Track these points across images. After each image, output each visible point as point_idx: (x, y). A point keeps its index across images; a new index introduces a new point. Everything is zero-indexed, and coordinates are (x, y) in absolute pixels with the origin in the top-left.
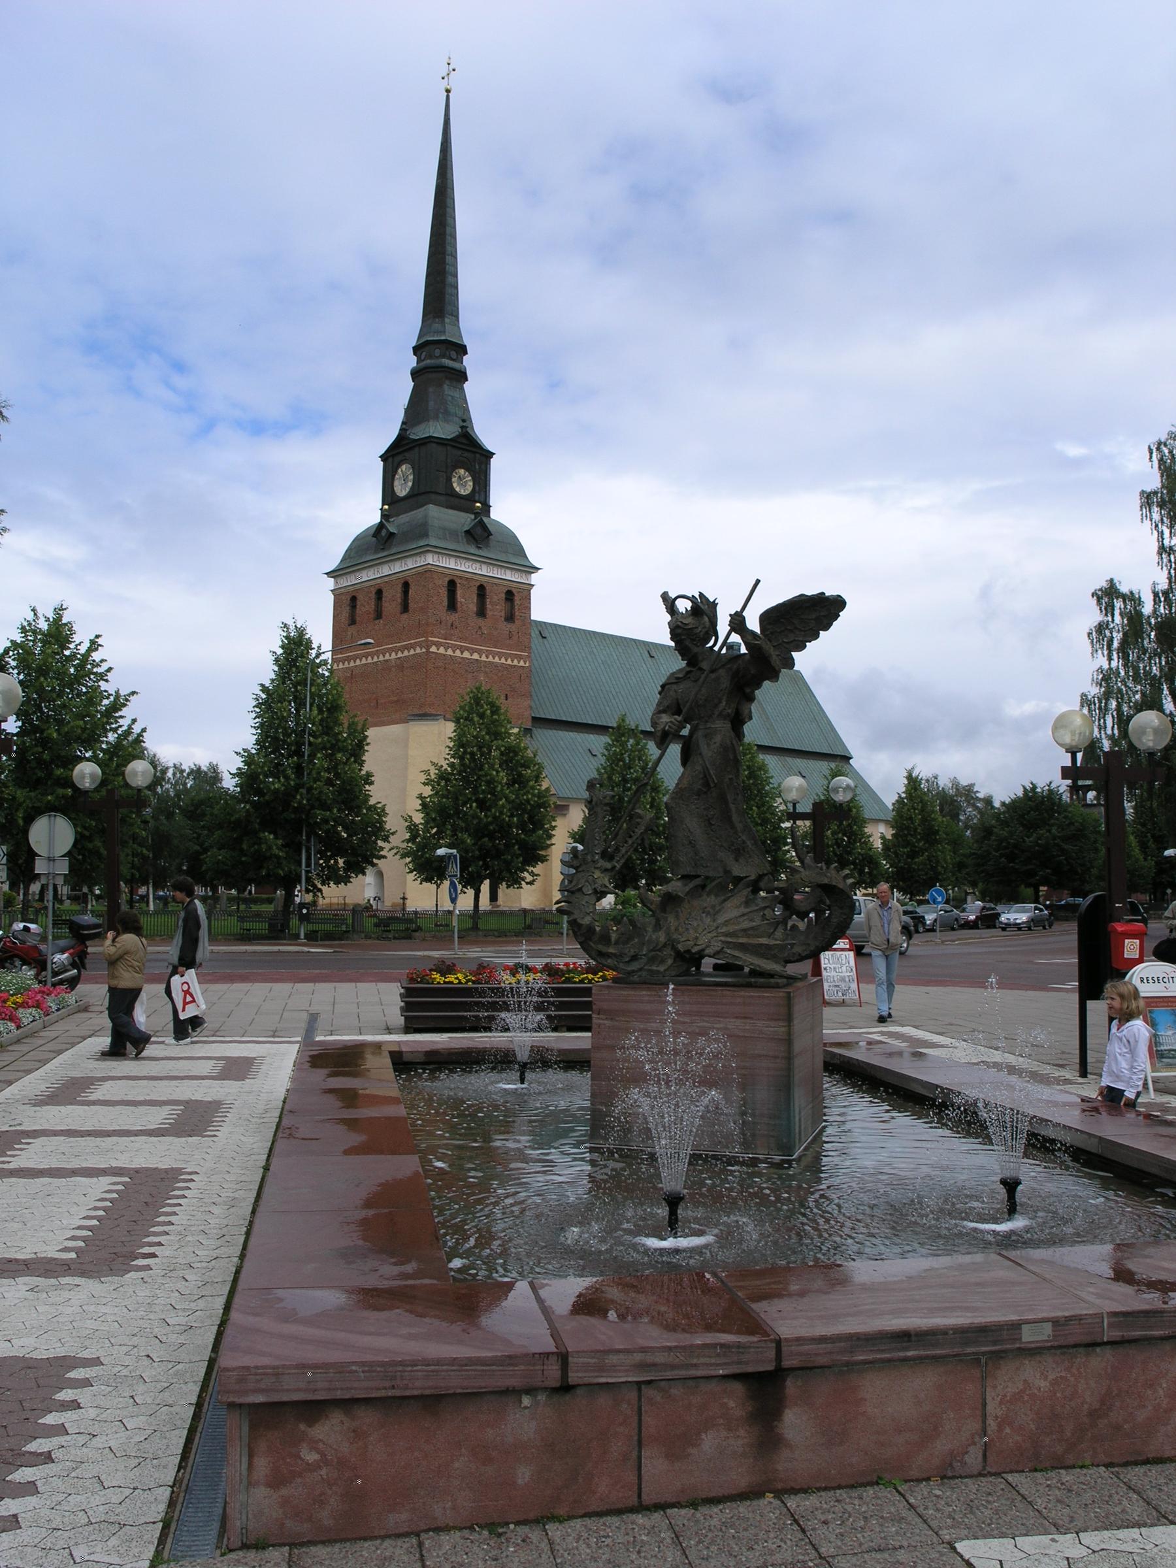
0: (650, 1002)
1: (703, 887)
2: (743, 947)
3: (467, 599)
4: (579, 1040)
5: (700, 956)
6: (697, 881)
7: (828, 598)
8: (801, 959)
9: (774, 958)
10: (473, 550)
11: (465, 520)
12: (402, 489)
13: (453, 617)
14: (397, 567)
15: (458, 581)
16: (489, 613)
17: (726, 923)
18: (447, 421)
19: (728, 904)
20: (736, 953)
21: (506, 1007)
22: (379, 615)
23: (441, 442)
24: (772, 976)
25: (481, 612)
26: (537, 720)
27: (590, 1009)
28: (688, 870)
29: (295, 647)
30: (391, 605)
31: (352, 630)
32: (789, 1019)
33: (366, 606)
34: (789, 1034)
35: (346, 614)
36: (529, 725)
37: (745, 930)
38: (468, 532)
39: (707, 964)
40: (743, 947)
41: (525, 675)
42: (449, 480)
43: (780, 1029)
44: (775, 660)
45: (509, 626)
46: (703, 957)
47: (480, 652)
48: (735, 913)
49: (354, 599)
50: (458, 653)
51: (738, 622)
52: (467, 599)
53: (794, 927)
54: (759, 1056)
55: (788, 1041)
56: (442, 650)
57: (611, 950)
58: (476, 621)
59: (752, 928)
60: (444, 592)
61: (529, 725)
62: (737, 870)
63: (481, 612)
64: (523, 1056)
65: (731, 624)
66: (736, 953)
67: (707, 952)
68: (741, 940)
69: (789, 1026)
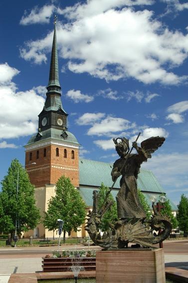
0: (113, 256)
1: (128, 221)
2: (140, 239)
3: (61, 153)
4: (92, 273)
5: (128, 242)
6: (125, 220)
7: (90, 76)
8: (157, 243)
9: (149, 242)
10: (63, 140)
11: (60, 132)
12: (44, 124)
13: (58, 158)
14: (43, 145)
15: (67, 149)
16: (67, 156)
17: (135, 232)
18: (56, 106)
19: (135, 226)
20: (138, 241)
21: (71, 265)
22: (38, 158)
23: (54, 112)
24: (149, 247)
25: (65, 156)
26: (80, 185)
27: (95, 265)
28: (124, 217)
29: (13, 168)
30: (41, 155)
31: (30, 162)
32: (155, 260)
33: (35, 155)
34: (155, 265)
35: (29, 158)
36: (79, 186)
37: (140, 234)
38: (61, 135)
39: (130, 245)
40: (140, 239)
41: (77, 173)
42: (56, 122)
43: (152, 263)
44: (146, 155)
45: (73, 160)
46: (128, 242)
47: (65, 167)
48: (137, 229)
49: (31, 153)
50: (59, 167)
51: (135, 145)
52: (61, 153)
53: (155, 233)
54: (146, 272)
55: (155, 267)
56: (55, 167)
57: (101, 241)
58: (64, 159)
59: (142, 233)
60: (55, 151)
61: (79, 186)
62: (137, 216)
63: (65, 156)
64: (99, 119)
65: (133, 145)
66: (138, 241)
67: (129, 240)
68: (139, 237)
69: (155, 263)
